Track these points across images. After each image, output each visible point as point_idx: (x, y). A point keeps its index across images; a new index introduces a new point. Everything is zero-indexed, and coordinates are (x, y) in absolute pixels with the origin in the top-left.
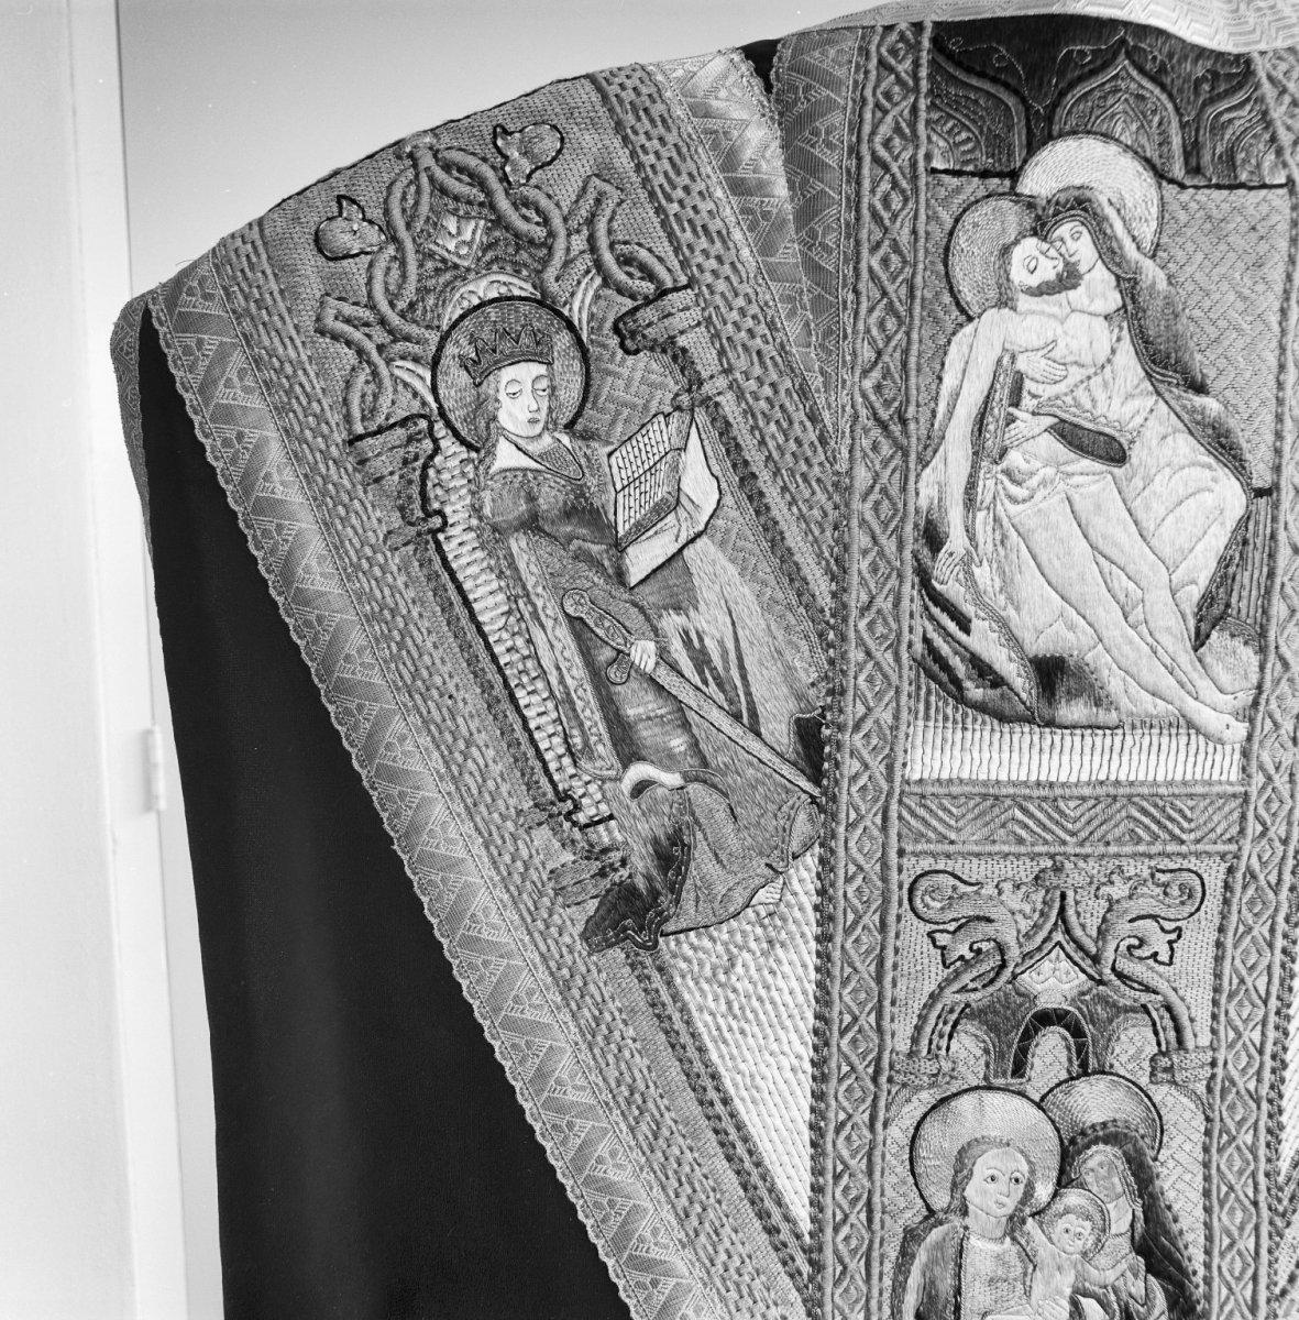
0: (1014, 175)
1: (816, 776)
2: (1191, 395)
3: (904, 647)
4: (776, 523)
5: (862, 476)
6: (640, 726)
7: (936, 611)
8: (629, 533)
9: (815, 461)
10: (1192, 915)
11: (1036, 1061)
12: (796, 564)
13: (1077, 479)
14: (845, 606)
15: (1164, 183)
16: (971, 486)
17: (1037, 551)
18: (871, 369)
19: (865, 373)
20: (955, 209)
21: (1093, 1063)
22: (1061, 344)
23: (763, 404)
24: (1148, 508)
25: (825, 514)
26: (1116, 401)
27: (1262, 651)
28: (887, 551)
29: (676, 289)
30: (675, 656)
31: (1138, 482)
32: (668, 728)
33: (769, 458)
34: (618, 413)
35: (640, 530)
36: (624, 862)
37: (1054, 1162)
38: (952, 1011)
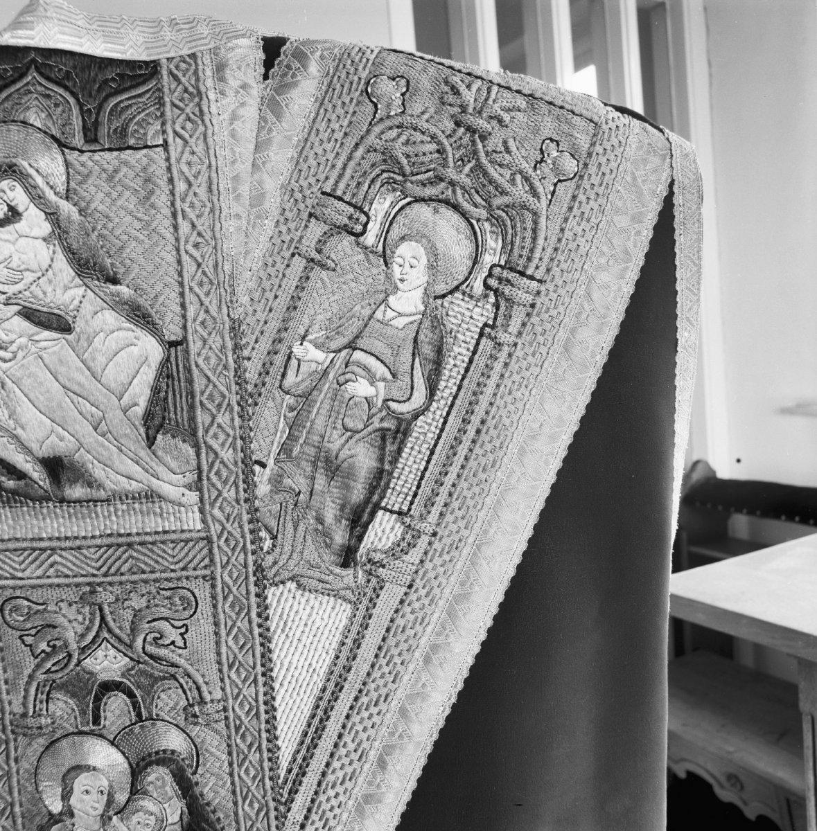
10: (192, 616)
11: (108, 714)
13: (42, 344)
15: (67, 151)
17: (26, 391)
21: (144, 714)
22: (15, 258)
24: (94, 359)
26: (59, 292)
37: (127, 779)
38: (44, 686)
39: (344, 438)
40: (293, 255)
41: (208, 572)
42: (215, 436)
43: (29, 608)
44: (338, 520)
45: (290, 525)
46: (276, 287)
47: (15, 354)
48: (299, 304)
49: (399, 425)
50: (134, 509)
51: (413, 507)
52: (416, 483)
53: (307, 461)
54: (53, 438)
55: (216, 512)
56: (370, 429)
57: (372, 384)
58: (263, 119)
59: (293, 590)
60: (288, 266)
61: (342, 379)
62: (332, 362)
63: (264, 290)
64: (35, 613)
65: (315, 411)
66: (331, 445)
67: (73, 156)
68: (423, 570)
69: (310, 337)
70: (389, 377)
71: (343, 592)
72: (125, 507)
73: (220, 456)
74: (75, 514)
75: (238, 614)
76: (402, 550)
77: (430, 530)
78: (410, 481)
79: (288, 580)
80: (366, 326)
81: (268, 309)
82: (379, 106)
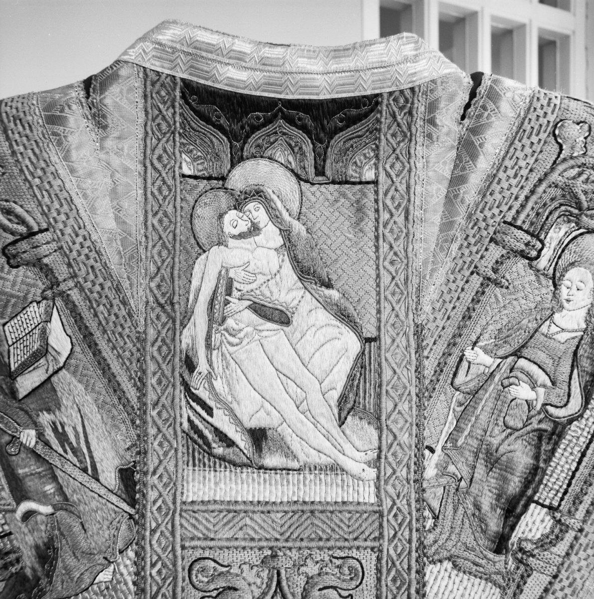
0: (224, 179)
1: (133, 503)
2: (323, 288)
3: (178, 425)
4: (105, 360)
5: (152, 333)
6: (27, 479)
7: (194, 404)
8: (17, 369)
9: (126, 326)
10: (357, 587)
12: (117, 382)
13: (264, 334)
14: (145, 404)
15: (302, 183)
16: (208, 338)
18: (155, 277)
19: (152, 279)
20: (195, 196)
22: (252, 264)
23: (95, 295)
24: (304, 349)
25: (132, 354)
27: (380, 429)
28: (166, 372)
29: (41, 231)
30: (48, 437)
31: (298, 335)
32: (44, 480)
33: (100, 323)
34: (8, 301)
35: (24, 367)
36: (18, 560)
39: (504, 434)
40: (472, 273)
41: (376, 544)
42: (396, 422)
43: (215, 569)
44: (493, 508)
45: (450, 508)
46: (455, 299)
47: (241, 340)
48: (473, 314)
49: (555, 428)
50: (320, 480)
51: (563, 503)
52: (567, 482)
53: (470, 451)
54: (262, 414)
55: (390, 488)
56: (529, 428)
57: (533, 388)
58: (459, 157)
59: (449, 570)
60: (467, 282)
61: (506, 382)
62: (498, 366)
63: (444, 302)
64: (219, 575)
65: (480, 408)
66: (492, 439)
67: (305, 186)
68: (569, 562)
69: (480, 344)
70: (549, 384)
71: (494, 577)
72: (312, 477)
73: (399, 438)
74: (270, 480)
75: (399, 588)
76: (551, 542)
77: (578, 526)
78: (562, 479)
79: (446, 559)
80: (531, 338)
81: (446, 317)
82: (564, 147)
